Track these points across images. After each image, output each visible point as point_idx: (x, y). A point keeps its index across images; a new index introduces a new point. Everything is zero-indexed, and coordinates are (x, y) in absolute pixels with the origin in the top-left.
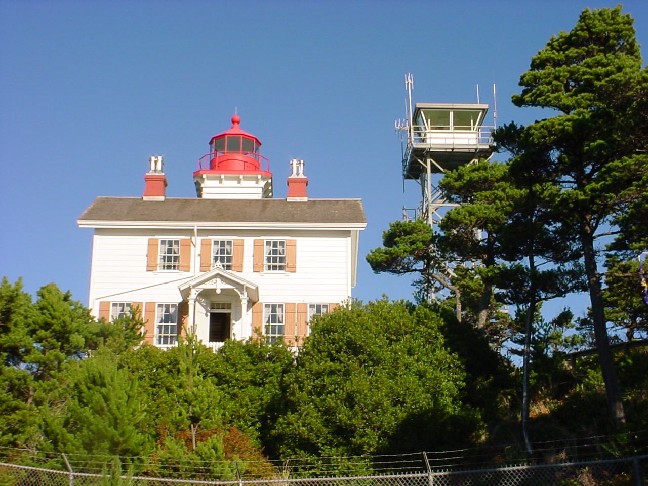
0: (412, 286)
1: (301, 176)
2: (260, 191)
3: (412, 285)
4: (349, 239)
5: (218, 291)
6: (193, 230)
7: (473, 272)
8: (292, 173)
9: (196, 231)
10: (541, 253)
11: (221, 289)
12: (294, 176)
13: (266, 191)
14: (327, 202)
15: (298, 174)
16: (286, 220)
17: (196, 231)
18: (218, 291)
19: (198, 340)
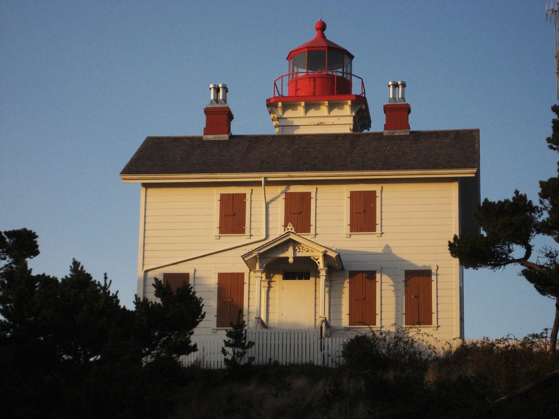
5: (291, 260)
18: (291, 260)
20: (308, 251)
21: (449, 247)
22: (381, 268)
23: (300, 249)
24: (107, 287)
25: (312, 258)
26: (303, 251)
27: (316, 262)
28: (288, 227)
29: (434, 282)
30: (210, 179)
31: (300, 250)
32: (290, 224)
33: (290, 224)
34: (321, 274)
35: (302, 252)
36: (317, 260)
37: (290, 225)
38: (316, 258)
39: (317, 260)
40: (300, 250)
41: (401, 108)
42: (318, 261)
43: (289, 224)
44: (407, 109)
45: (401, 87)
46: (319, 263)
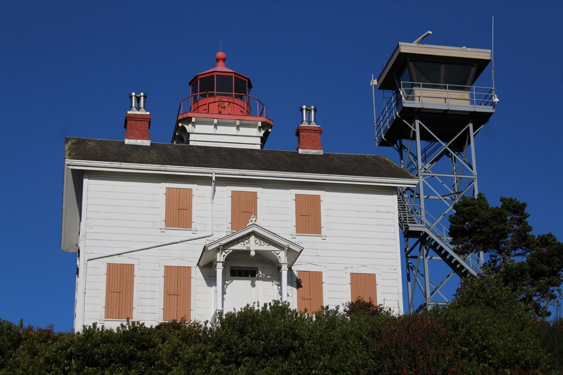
0: (240, 309)
1: (313, 125)
2: (258, 141)
3: (241, 308)
4: (211, 187)
5: (253, 253)
6: (212, 177)
7: (522, 309)
8: (303, 121)
9: (214, 179)
10: (499, 269)
11: (255, 251)
12: (305, 124)
13: (263, 140)
14: (115, 142)
15: (310, 122)
16: (183, 164)
17: (214, 179)
18: (253, 253)
19: (53, 329)
20: (261, 245)
21: (541, 235)
22: (225, 273)
23: (261, 243)
24: (420, 243)
25: (272, 252)
26: (264, 245)
27: (277, 256)
28: (252, 219)
29: (103, 306)
30: (433, 148)
31: (261, 244)
32: (253, 216)
33: (253, 216)
34: (283, 268)
35: (263, 245)
36: (278, 254)
37: (253, 217)
38: (278, 252)
39: (278, 254)
40: (261, 244)
41: (314, 130)
42: (279, 255)
43: (252, 216)
44: (148, 120)
45: (305, 111)
46: (280, 257)
